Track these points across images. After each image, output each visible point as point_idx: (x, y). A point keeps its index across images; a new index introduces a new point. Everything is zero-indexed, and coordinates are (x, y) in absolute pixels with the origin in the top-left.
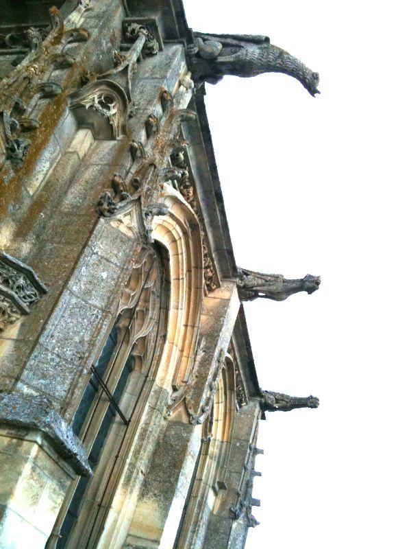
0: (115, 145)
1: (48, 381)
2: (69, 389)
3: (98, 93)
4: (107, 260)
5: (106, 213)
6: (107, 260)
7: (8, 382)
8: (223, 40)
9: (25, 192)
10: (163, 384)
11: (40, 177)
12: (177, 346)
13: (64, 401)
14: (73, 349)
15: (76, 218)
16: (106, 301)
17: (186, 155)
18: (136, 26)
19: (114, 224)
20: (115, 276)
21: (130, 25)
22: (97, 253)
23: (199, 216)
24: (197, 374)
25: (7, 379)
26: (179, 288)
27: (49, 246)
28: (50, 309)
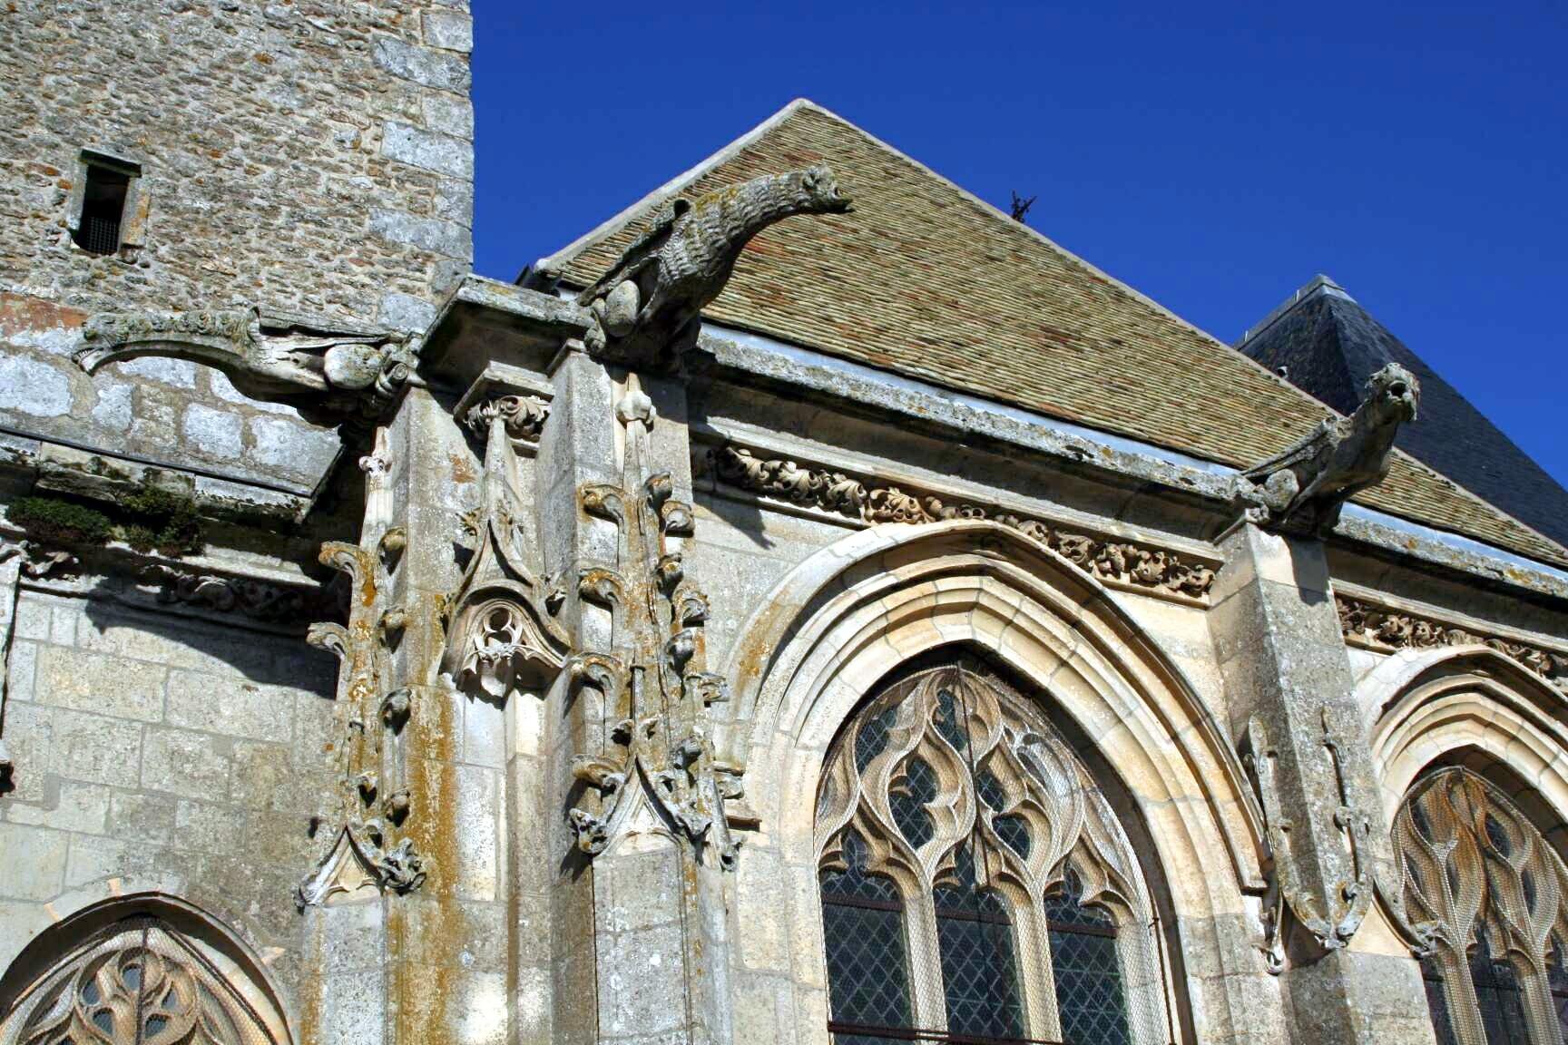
3: (476, 624)
4: (647, 928)
5: (593, 848)
6: (647, 928)
9: (475, 910)
10: (1210, 908)
11: (489, 855)
12: (1185, 798)
17: (802, 464)
19: (624, 849)
20: (677, 946)
22: (624, 930)
23: (977, 514)
24: (1283, 821)
26: (1085, 681)
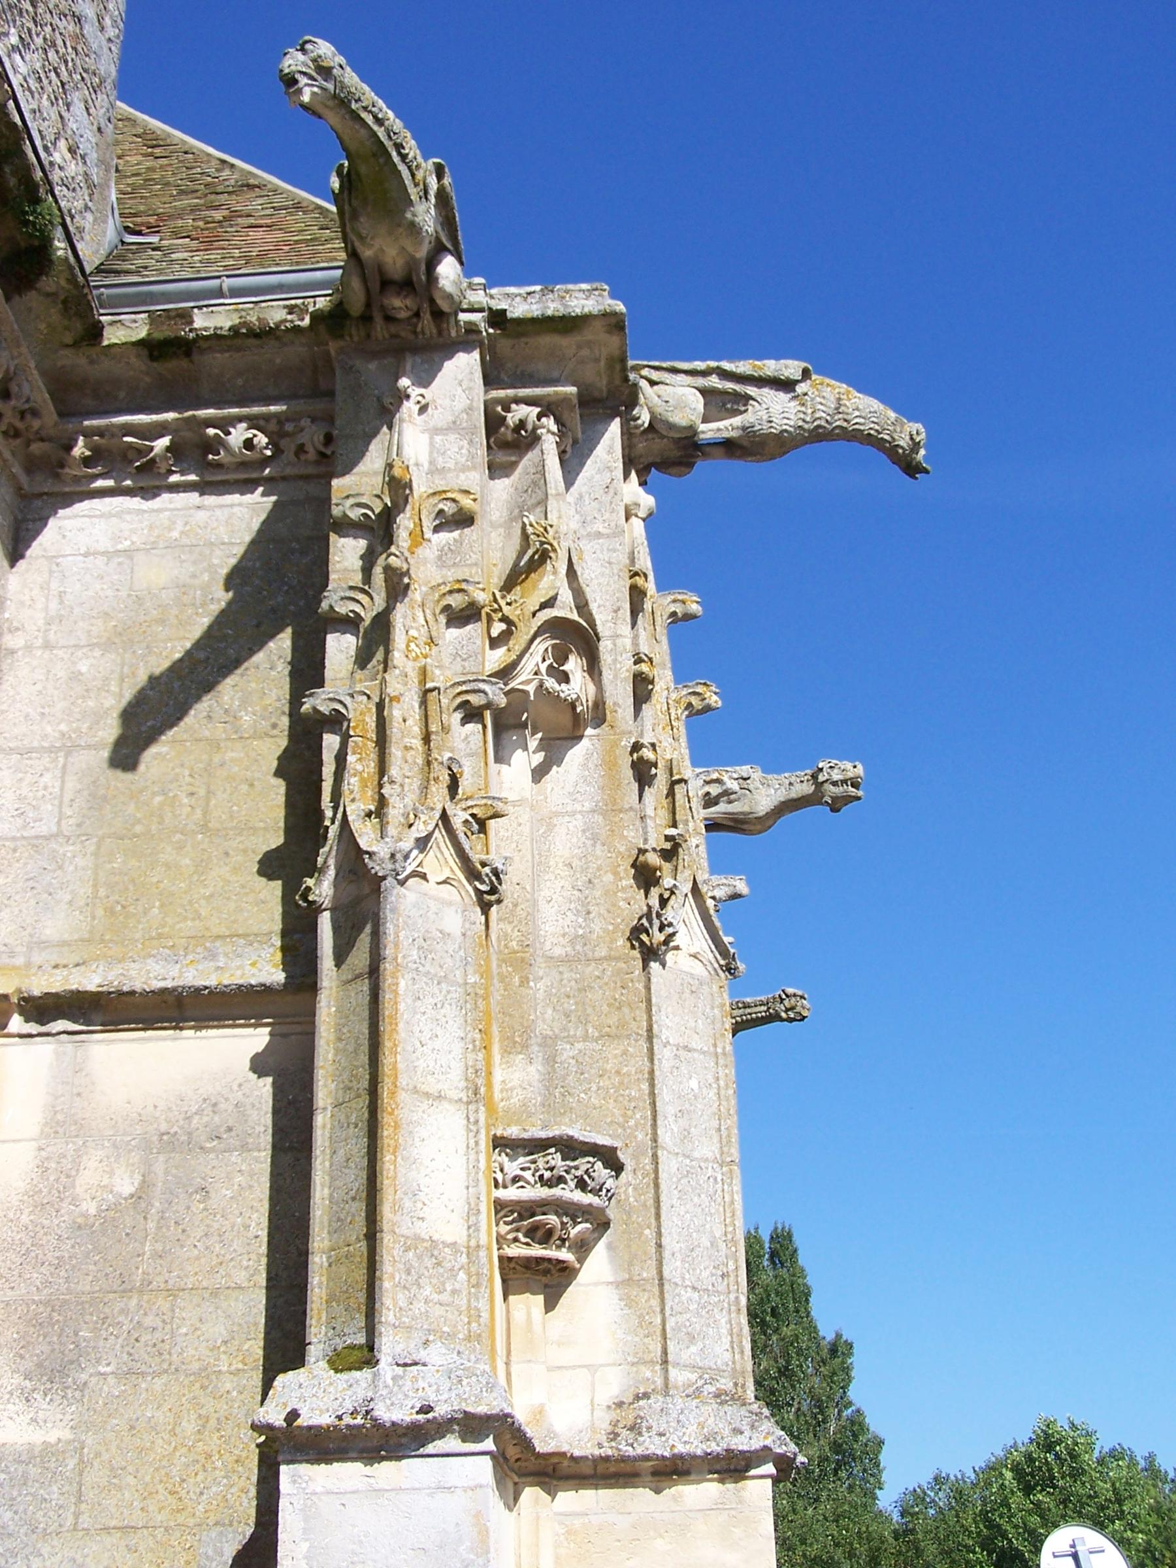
0: (588, 756)
1: (700, 1345)
2: (732, 1342)
7: (648, 1374)
8: (701, 382)
13: (734, 1369)
14: (707, 1263)
15: (592, 970)
16: (716, 1139)
18: (521, 412)
21: (507, 409)
25: (643, 1368)
27: (567, 1052)
28: (651, 1202)
